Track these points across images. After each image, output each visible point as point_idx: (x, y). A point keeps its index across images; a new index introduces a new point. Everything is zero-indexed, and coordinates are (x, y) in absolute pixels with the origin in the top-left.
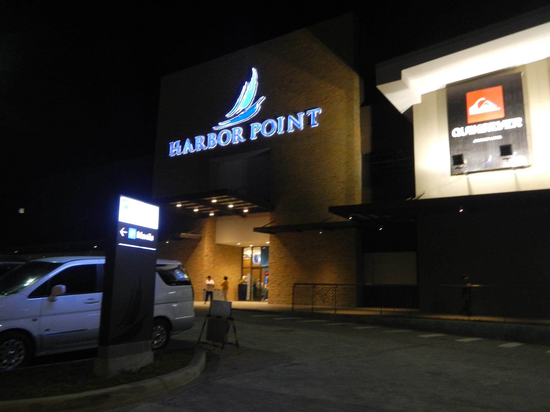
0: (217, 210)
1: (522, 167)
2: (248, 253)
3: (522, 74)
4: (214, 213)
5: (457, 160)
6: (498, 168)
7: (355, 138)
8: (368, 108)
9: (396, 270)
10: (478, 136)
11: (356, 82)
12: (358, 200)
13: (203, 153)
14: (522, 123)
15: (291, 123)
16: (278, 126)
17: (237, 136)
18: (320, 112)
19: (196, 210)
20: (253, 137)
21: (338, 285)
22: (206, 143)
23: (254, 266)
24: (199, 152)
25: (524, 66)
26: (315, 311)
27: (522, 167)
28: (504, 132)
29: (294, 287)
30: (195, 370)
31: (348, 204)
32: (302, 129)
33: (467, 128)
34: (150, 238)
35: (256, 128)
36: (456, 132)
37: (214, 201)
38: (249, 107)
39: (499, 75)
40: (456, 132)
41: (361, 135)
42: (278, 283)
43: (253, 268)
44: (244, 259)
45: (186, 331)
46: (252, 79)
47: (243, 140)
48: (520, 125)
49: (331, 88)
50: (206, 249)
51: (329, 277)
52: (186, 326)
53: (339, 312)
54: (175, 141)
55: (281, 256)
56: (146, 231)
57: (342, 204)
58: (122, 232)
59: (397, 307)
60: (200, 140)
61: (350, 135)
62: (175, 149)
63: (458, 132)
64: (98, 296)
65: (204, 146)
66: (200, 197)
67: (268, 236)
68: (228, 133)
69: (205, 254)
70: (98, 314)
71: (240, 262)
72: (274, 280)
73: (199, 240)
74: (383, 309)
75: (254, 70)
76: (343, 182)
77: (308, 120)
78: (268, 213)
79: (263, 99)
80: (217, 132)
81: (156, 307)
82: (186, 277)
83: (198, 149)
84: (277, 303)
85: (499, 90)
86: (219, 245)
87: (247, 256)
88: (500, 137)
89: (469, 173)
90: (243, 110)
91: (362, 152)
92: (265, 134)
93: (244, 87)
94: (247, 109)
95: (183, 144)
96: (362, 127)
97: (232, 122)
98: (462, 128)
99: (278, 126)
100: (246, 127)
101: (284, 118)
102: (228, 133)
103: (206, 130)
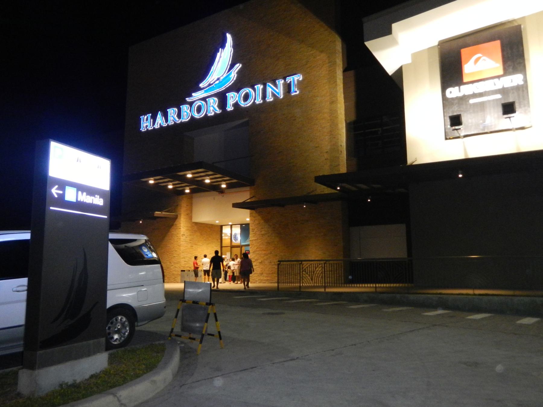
0: (194, 187)
1: (523, 128)
2: (226, 231)
3: (522, 26)
4: (190, 189)
5: (456, 121)
6: (497, 129)
7: (339, 105)
8: (351, 73)
9: (386, 243)
10: (474, 96)
11: (338, 45)
12: (343, 169)
13: (176, 127)
14: (523, 80)
15: (269, 90)
16: (255, 95)
17: (213, 108)
18: (301, 79)
19: (170, 187)
20: (230, 108)
21: (326, 261)
22: (179, 116)
23: (233, 244)
24: (172, 126)
25: (523, 18)
26: (302, 290)
27: (523, 128)
28: (504, 91)
29: (278, 264)
30: (164, 376)
31: (332, 173)
32: (282, 97)
33: (462, 87)
34: (99, 201)
35: (232, 98)
36: (451, 92)
37: (189, 176)
38: (225, 76)
39: (497, 29)
40: (451, 92)
41: (345, 102)
42: (260, 261)
43: (232, 247)
44: (223, 238)
45: (158, 320)
46: (227, 45)
47: (218, 111)
48: (521, 83)
49: (312, 52)
50: (183, 227)
51: (314, 252)
52: (155, 314)
53: (328, 290)
54: (145, 114)
55: (263, 232)
56: (91, 191)
57: (326, 173)
58: (55, 191)
59: (394, 283)
60: (172, 112)
61: (333, 102)
62: (146, 124)
63: (453, 92)
64: (24, 281)
65: (177, 119)
66: (173, 172)
67: (248, 211)
68: (202, 103)
69: (182, 233)
70: (23, 307)
71: (220, 241)
72: (256, 258)
73: (176, 218)
74: (377, 285)
75: (229, 37)
76: (327, 152)
77: (288, 88)
78: (248, 188)
79: (238, 66)
80: (191, 104)
81: (109, 294)
82: (154, 255)
83: (171, 122)
84: (260, 283)
85: (497, 44)
86: (196, 223)
87: (226, 235)
88: (499, 96)
89: (465, 136)
90: (218, 79)
91: (346, 120)
92: (242, 104)
93: (219, 54)
94: (222, 78)
95: (154, 118)
96: (345, 93)
97: (206, 91)
98: (457, 88)
99: (255, 95)
100: (222, 97)
101: (262, 87)
102: (202, 103)
103: (178, 102)
